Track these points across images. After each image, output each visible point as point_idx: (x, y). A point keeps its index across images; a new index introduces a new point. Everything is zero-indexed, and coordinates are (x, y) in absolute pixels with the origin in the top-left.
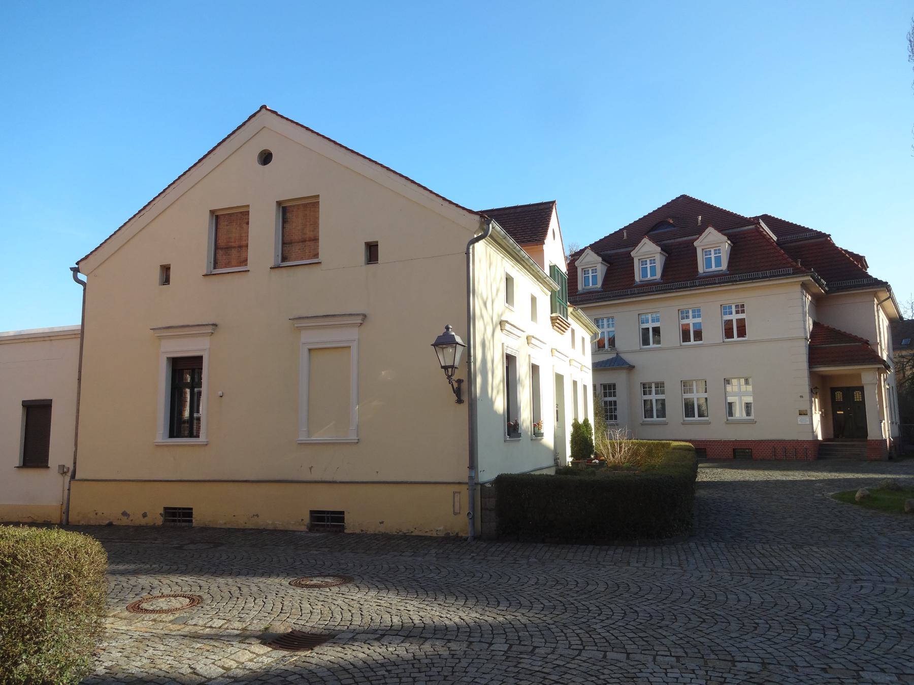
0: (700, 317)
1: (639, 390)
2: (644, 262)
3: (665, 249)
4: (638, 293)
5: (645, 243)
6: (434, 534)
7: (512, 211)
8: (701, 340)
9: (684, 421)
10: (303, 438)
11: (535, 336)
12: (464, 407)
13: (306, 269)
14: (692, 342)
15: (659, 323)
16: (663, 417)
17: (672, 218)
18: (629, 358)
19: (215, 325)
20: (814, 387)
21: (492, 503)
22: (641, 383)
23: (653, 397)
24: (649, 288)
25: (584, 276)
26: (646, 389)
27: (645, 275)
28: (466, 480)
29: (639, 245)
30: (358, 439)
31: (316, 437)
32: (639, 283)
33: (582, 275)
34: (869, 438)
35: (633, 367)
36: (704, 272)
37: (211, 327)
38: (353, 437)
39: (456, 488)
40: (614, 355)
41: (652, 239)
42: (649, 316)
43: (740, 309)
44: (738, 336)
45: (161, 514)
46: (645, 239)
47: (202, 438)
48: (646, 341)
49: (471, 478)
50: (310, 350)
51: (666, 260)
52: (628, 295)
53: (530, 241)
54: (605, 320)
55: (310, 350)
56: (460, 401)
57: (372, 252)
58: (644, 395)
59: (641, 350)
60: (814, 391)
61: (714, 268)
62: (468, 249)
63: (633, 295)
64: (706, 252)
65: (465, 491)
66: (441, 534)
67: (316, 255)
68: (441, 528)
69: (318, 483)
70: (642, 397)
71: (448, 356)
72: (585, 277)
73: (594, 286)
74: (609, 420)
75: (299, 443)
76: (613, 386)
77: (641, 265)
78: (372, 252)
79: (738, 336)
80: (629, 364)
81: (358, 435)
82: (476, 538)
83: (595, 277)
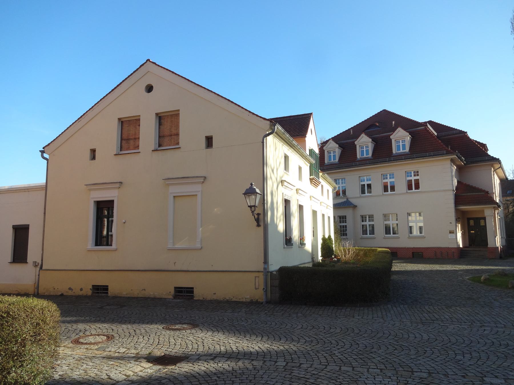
0: (394, 178)
1: (359, 219)
2: (362, 148)
3: (374, 140)
4: (359, 165)
5: (363, 137)
6: (244, 300)
7: (288, 118)
8: (394, 191)
9: (385, 237)
10: (170, 246)
11: (301, 189)
12: (261, 229)
13: (172, 151)
14: (389, 192)
15: (371, 181)
16: (373, 235)
17: (378, 122)
18: (354, 201)
19: (121, 183)
20: (458, 218)
21: (277, 283)
22: (360, 215)
23: (367, 223)
24: (365, 162)
25: (328, 155)
26: (363, 219)
27: (363, 154)
28: (262, 270)
29: (359, 138)
30: (202, 247)
31: (178, 246)
32: (359, 159)
33: (327, 155)
34: (489, 246)
35: (356, 206)
36: (396, 153)
37: (119, 184)
38: (198, 246)
39: (257, 274)
40: (345, 200)
41: (367, 134)
42: (365, 178)
43: (416, 174)
44: (415, 189)
45: (90, 289)
46: (362, 134)
47: (114, 246)
48: (363, 192)
49: (265, 268)
50: (174, 197)
51: (375, 146)
52: (353, 166)
53: (298, 135)
54: (340, 180)
55: (174, 197)
56: (259, 225)
57: (209, 141)
58: (362, 222)
59: (360, 197)
60: (458, 220)
61: (401, 151)
62: (263, 140)
63: (356, 166)
64: (397, 141)
65: (261, 276)
66: (248, 300)
67: (178, 144)
68: (248, 297)
69: (179, 271)
70: (361, 223)
71: (252, 200)
72: (329, 156)
73: (334, 161)
74: (342, 236)
75: (168, 249)
76: (345, 217)
77: (360, 149)
78: (209, 141)
79: (415, 189)
80: (354, 205)
81: (201, 245)
82: (268, 302)
83: (334, 156)
